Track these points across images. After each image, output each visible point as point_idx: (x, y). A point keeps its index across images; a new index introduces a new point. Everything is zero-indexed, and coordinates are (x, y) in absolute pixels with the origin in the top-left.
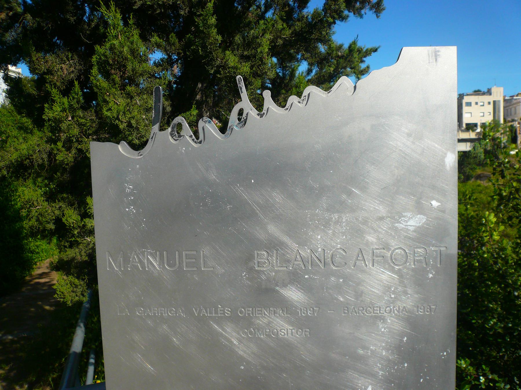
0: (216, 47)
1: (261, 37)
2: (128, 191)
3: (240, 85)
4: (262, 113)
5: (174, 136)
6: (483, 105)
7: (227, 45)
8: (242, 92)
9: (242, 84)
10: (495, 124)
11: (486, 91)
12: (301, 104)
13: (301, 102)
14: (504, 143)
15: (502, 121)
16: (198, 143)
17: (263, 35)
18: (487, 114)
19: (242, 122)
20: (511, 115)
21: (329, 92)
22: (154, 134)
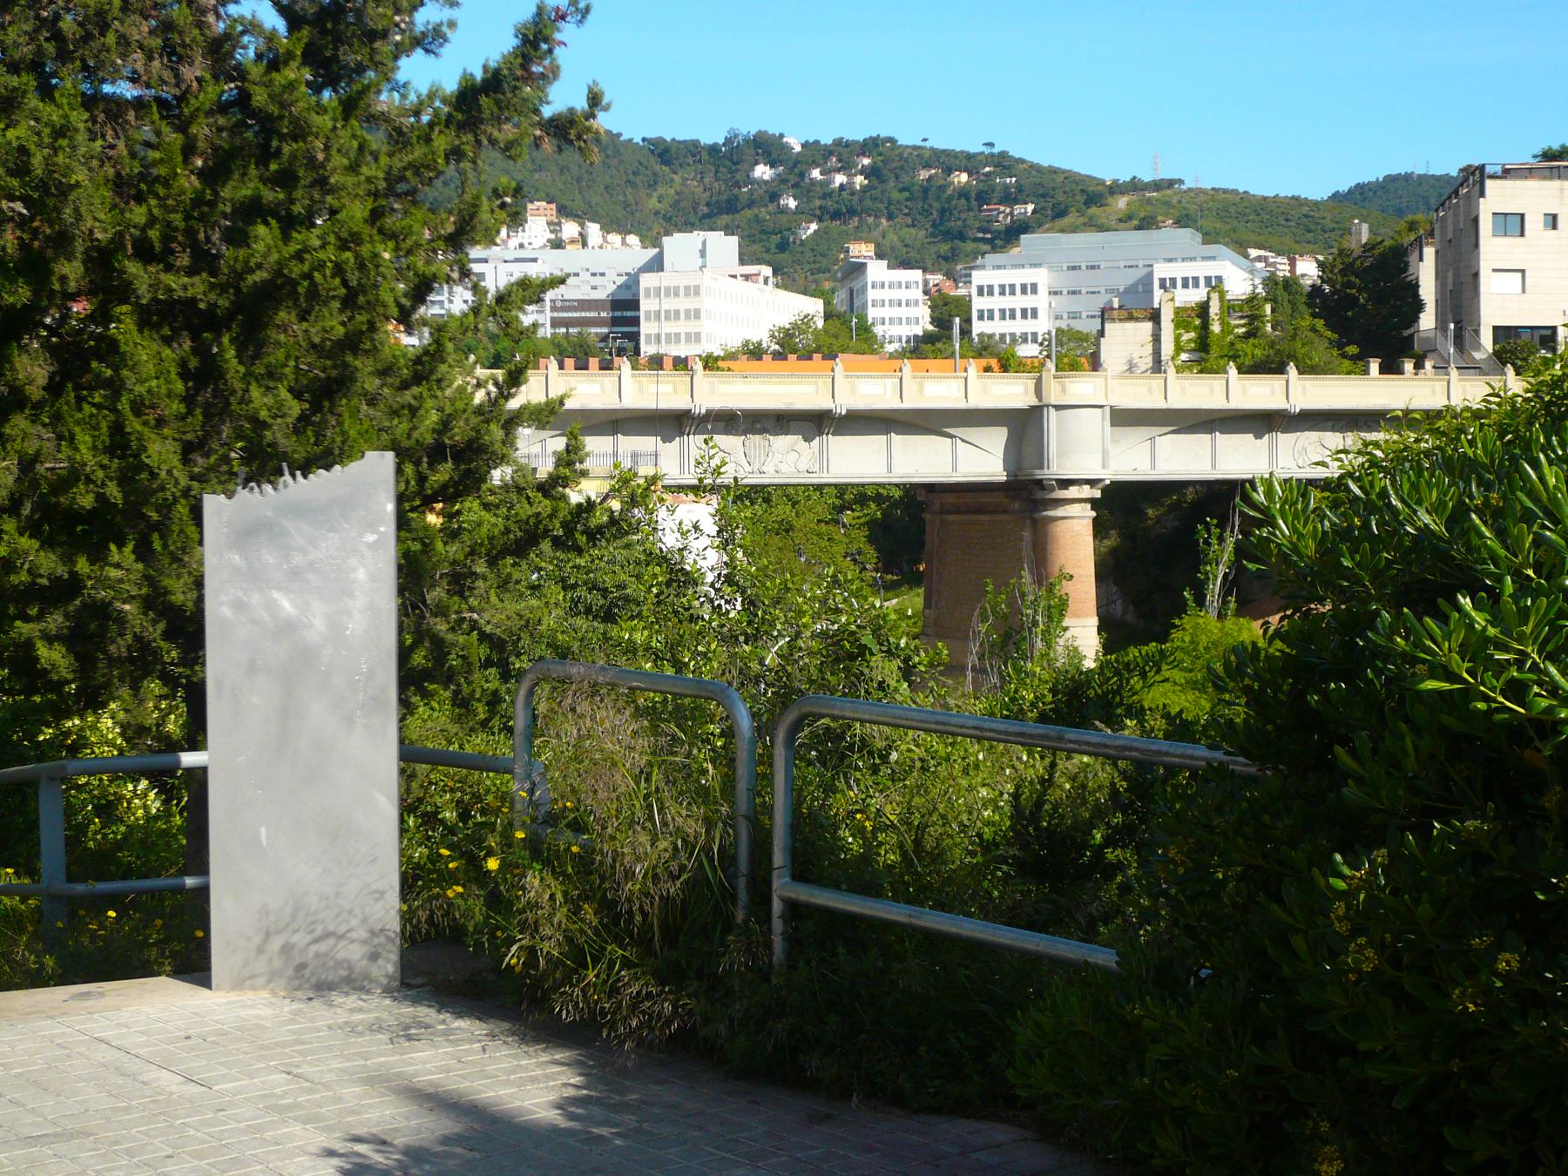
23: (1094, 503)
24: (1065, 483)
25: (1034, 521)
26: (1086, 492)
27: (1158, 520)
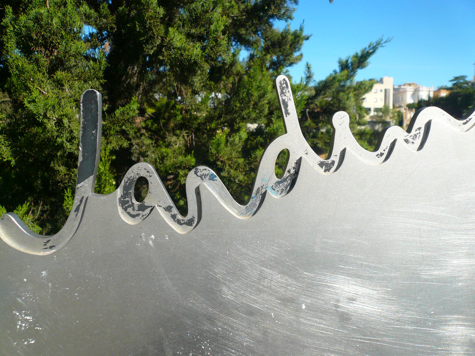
0: (157, 22)
1: (212, 11)
2: (21, 326)
3: (284, 98)
4: (330, 161)
5: (129, 206)
6: (376, 92)
8: (287, 113)
9: (288, 94)
10: (385, 110)
11: (379, 80)
12: (410, 144)
13: (411, 140)
15: (391, 107)
16: (184, 223)
17: (214, 8)
19: (285, 180)
20: (399, 101)
21: (465, 121)
22: (81, 201)
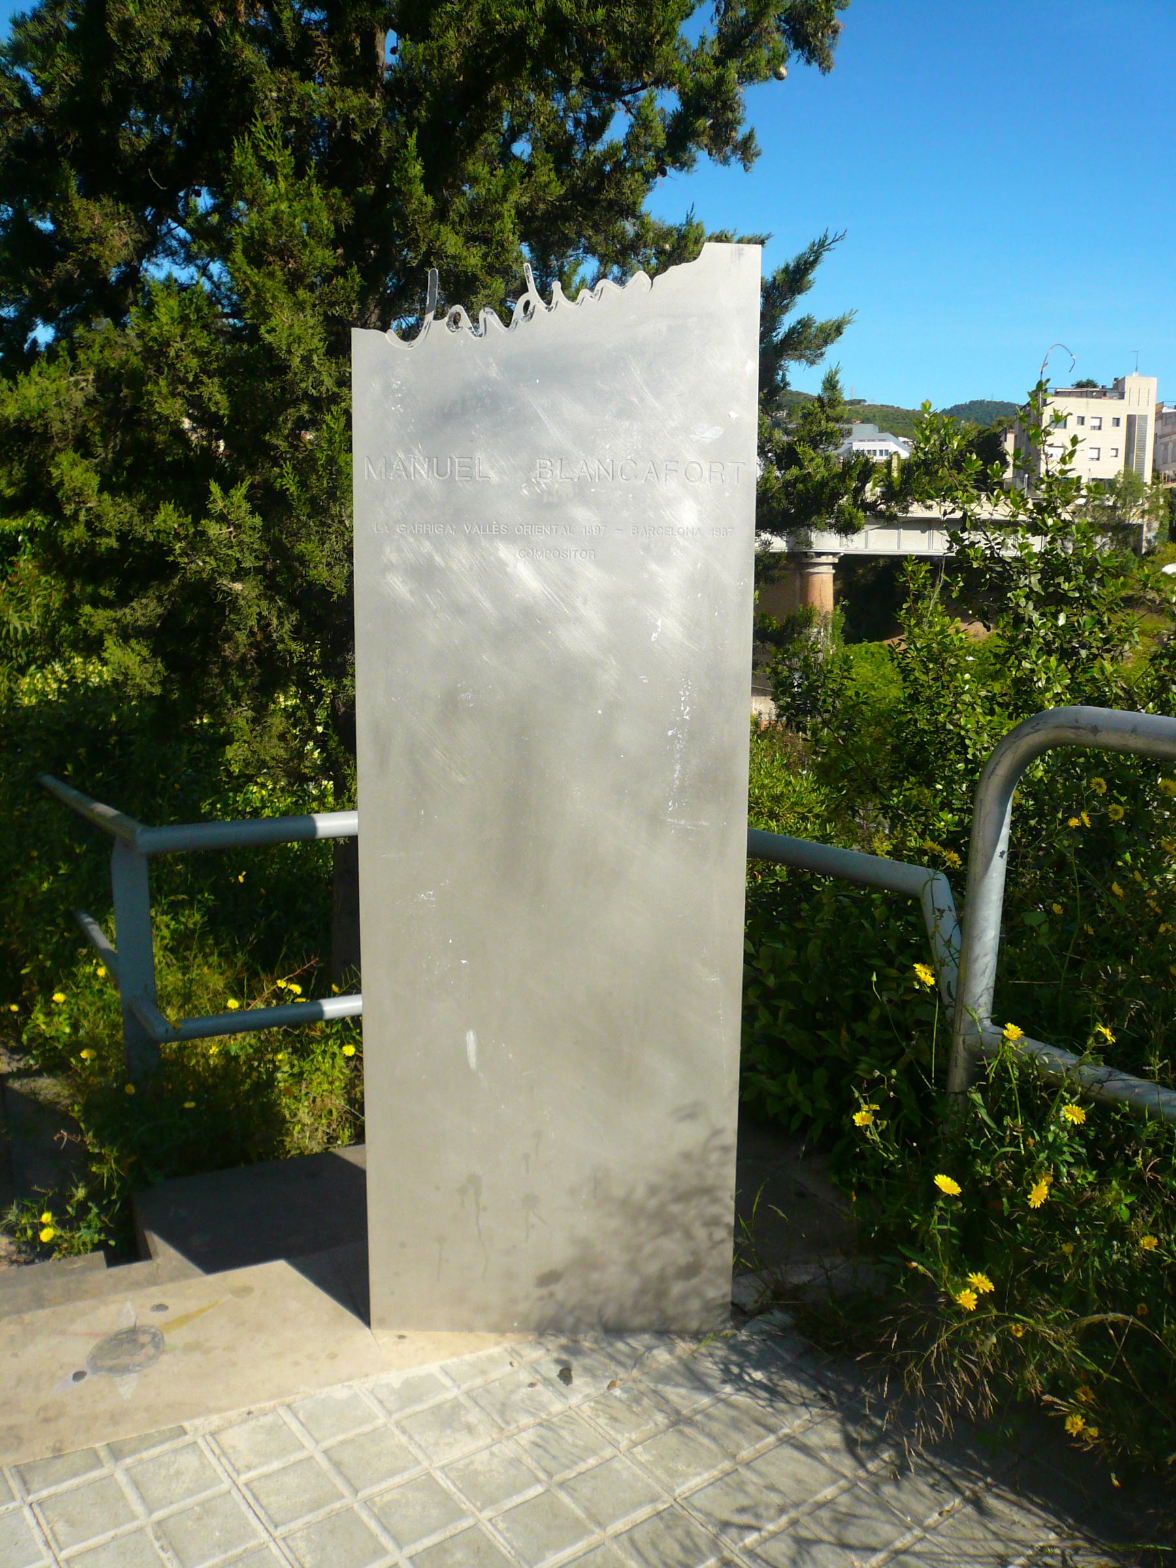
7: (441, 214)
11: (1110, 386)
14: (1149, 541)
15: (1148, 477)
18: (1106, 454)
23: (834, 565)
24: (820, 554)
25: (801, 575)
26: (831, 559)
27: (863, 576)
